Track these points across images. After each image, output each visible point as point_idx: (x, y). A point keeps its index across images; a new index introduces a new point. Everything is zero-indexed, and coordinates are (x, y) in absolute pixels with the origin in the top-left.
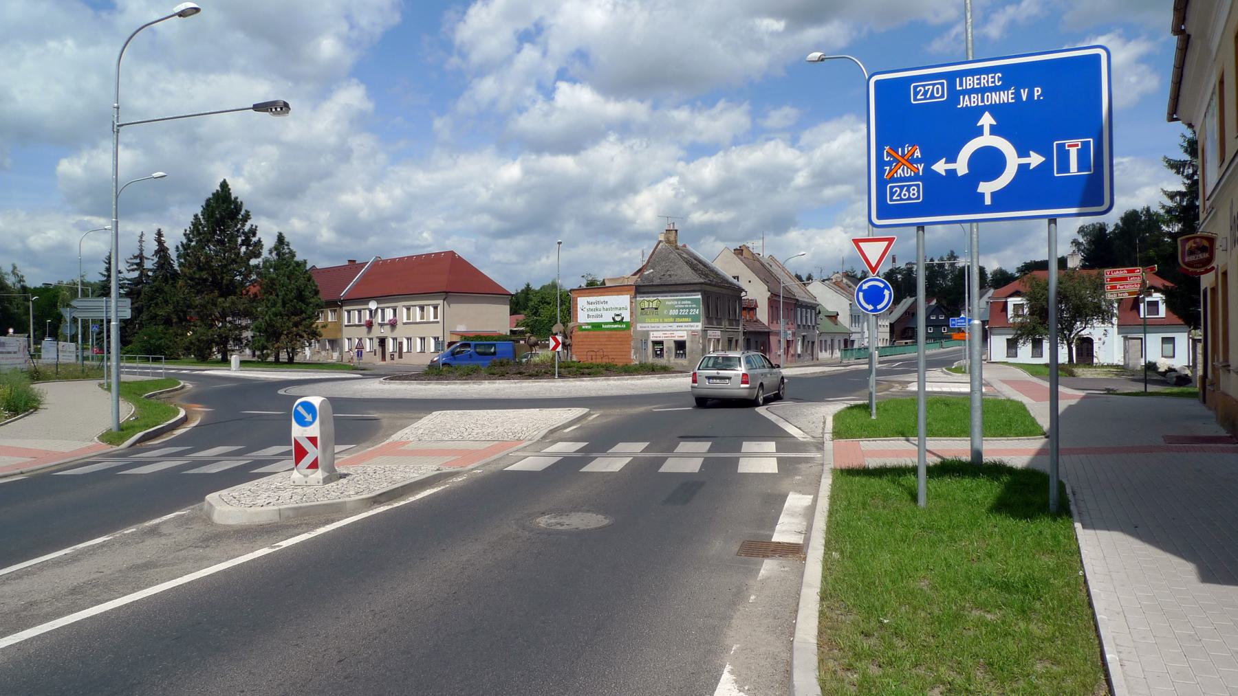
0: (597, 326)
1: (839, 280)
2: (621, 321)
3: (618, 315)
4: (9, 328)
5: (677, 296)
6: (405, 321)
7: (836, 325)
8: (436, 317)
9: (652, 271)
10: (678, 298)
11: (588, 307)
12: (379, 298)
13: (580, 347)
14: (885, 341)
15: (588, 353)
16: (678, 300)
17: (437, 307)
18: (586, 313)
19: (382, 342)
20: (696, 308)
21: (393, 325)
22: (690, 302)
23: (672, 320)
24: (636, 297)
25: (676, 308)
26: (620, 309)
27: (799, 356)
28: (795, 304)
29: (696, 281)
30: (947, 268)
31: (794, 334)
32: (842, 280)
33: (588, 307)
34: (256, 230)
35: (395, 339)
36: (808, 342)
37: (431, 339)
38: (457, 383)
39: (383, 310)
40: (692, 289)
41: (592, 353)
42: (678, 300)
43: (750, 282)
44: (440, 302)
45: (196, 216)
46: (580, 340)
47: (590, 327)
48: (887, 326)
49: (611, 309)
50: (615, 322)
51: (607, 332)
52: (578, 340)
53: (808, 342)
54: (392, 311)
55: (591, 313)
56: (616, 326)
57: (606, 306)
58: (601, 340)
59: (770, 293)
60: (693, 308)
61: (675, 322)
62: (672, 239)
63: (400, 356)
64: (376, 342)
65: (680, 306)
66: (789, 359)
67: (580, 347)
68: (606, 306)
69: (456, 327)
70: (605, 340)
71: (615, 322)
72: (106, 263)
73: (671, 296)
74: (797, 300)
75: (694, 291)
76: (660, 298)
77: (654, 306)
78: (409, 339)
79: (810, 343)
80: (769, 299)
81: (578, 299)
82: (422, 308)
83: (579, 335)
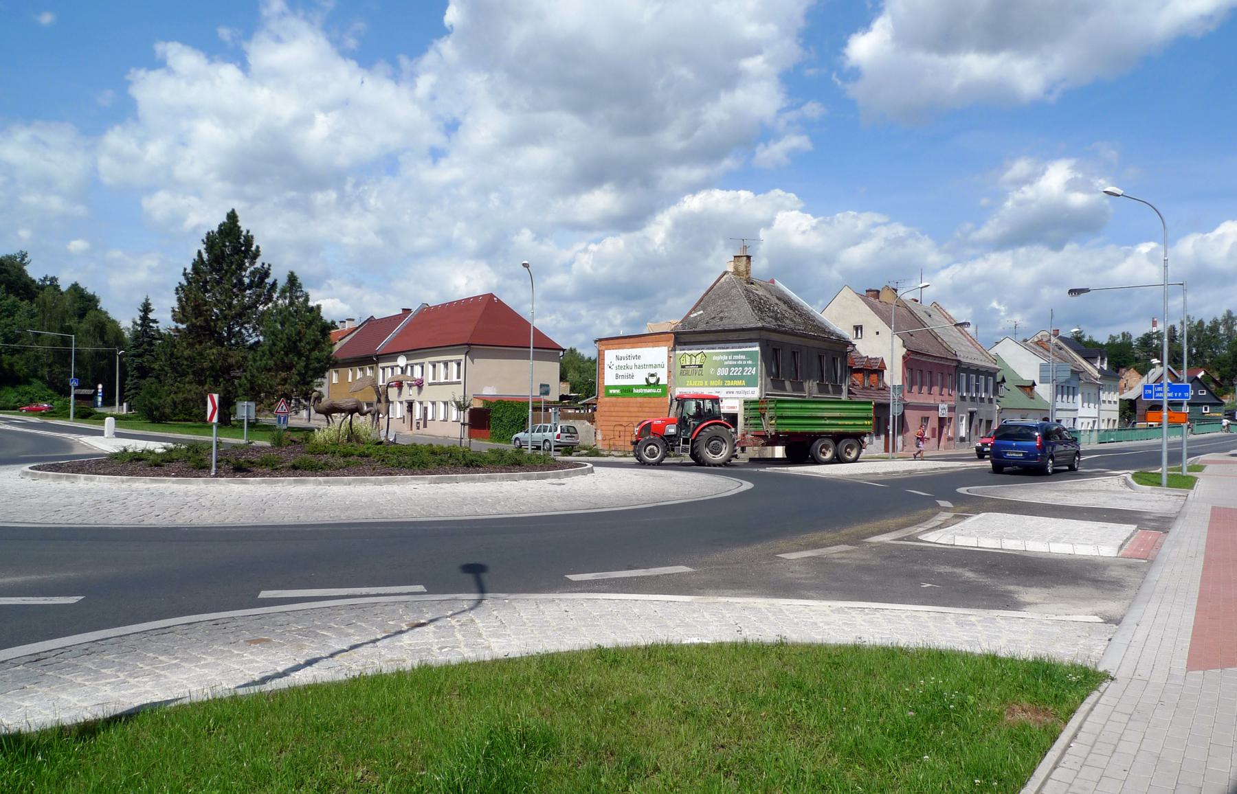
0: (627, 390)
1: (1045, 339)
2: (656, 384)
3: (652, 375)
4: (100, 383)
5: (727, 348)
6: (431, 381)
7: (1033, 398)
8: (459, 377)
9: (702, 312)
10: (728, 350)
11: (617, 363)
12: (409, 353)
13: (607, 418)
14: (1111, 422)
15: (616, 428)
16: (728, 354)
17: (460, 363)
18: (614, 372)
19: (410, 406)
20: (752, 366)
21: (420, 385)
22: (743, 357)
23: (720, 382)
24: (675, 350)
25: (726, 366)
26: (656, 366)
27: (962, 440)
28: (957, 366)
29: (752, 325)
30: (1222, 332)
31: (951, 409)
32: (1050, 340)
33: (617, 363)
34: (269, 269)
35: (421, 403)
36: (981, 420)
37: (441, 403)
38: (47, 476)
39: (412, 367)
40: (747, 337)
41: (622, 428)
42: (728, 354)
43: (878, 333)
44: (462, 357)
45: (199, 252)
46: (606, 409)
47: (618, 391)
48: (1115, 402)
49: (644, 366)
50: (649, 385)
51: (639, 399)
52: (604, 409)
53: (981, 420)
54: (420, 369)
55: (621, 372)
56: (649, 391)
57: (638, 362)
58: (631, 409)
59: (905, 350)
60: (748, 366)
61: (724, 386)
62: (742, 268)
63: (425, 426)
64: (406, 405)
65: (731, 363)
66: (942, 443)
67: (607, 418)
68: (638, 362)
69: (482, 390)
70: (636, 409)
71: (649, 385)
72: (140, 310)
73: (720, 348)
74: (959, 362)
75: (751, 340)
76: (705, 351)
77: (698, 363)
78: (434, 403)
79: (984, 423)
80: (904, 357)
81: (606, 352)
82: (446, 364)
83: (606, 403)
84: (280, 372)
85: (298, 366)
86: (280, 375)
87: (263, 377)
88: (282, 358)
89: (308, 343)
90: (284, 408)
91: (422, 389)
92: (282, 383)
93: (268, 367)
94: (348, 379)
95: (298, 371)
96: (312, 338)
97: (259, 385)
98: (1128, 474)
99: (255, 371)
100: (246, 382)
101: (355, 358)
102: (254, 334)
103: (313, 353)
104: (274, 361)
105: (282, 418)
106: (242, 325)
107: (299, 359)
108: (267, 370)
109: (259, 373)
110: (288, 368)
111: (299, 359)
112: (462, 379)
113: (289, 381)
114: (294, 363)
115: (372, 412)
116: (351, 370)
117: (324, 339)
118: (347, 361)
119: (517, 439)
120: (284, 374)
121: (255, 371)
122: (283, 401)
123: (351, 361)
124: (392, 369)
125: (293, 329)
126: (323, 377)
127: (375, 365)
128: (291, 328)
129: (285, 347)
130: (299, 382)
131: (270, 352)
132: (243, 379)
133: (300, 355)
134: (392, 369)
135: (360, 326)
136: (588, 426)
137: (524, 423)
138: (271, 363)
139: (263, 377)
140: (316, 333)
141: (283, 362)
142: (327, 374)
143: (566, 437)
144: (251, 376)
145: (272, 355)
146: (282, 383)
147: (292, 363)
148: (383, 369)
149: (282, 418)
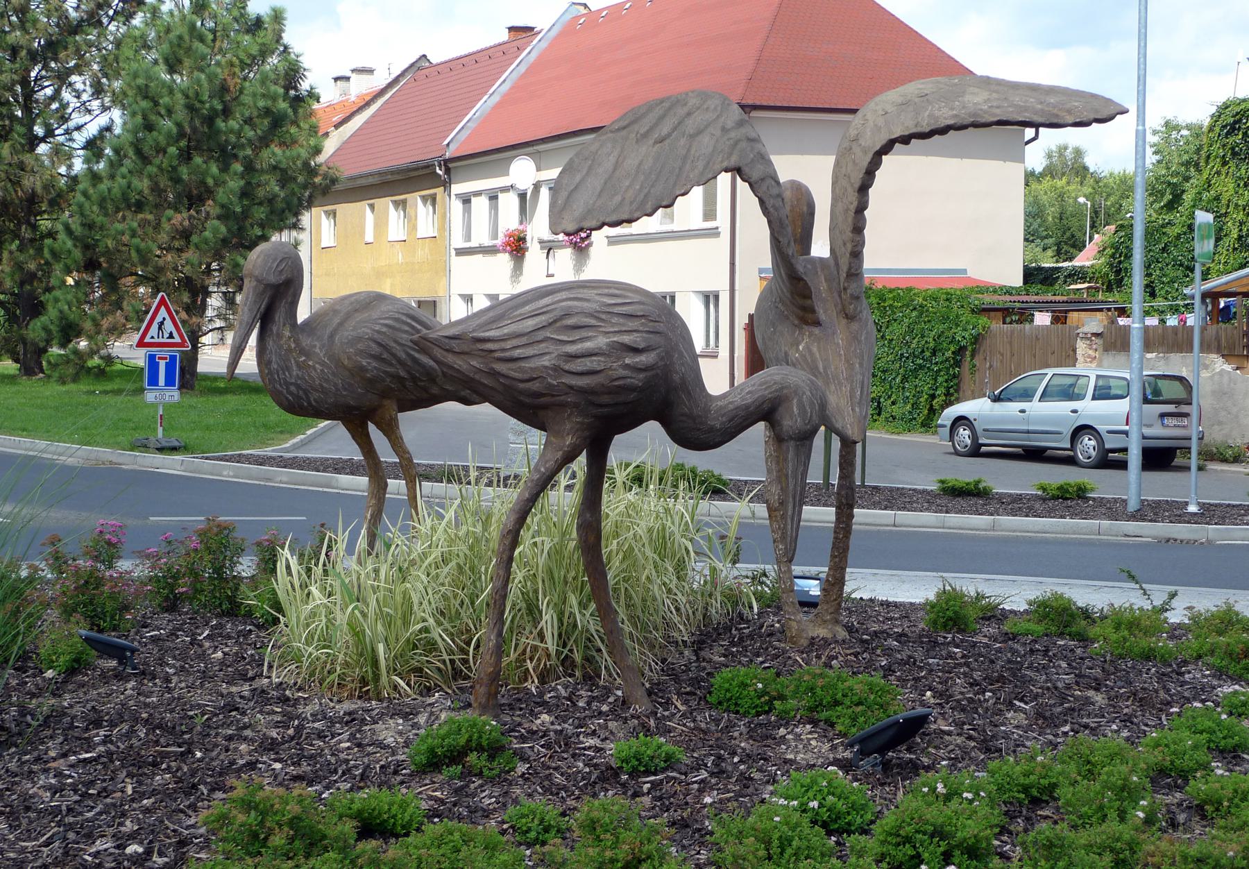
8: (710, 213)
37: (693, 296)
84: (170, 212)
85: (221, 195)
86: (169, 220)
87: (119, 226)
88: (174, 169)
89: (249, 121)
90: (169, 327)
91: (587, 256)
92: (177, 244)
93: (134, 197)
94: (362, 233)
95: (223, 206)
96: (261, 104)
97: (108, 252)
98: (501, 298)
99: (94, 212)
100: (69, 243)
101: (380, 174)
102: (95, 104)
103: (265, 154)
104: (150, 177)
105: (162, 364)
106: (62, 78)
107: (225, 168)
108: (129, 207)
109: (106, 215)
110: (195, 197)
111: (225, 168)
112: (722, 220)
113: (195, 238)
114: (210, 181)
115: (791, 420)
116: (372, 207)
117: (295, 112)
118: (363, 182)
119: (961, 420)
120: (180, 218)
121: (95, 208)
122: (162, 302)
123: (371, 180)
124: (493, 198)
125: (203, 76)
126: (295, 226)
127: (439, 191)
128: (196, 73)
129: (181, 134)
130: (225, 242)
131: (139, 152)
132: (62, 236)
133: (225, 156)
134: (493, 198)
135: (390, 85)
136: (1222, 372)
137: (958, 364)
138: (143, 185)
139: (119, 226)
140: (273, 88)
141: (177, 180)
142: (305, 219)
143: (1163, 415)
144: (83, 225)
145: (144, 158)
146: (177, 244)
147: (203, 183)
148: (466, 200)
149: (162, 364)
